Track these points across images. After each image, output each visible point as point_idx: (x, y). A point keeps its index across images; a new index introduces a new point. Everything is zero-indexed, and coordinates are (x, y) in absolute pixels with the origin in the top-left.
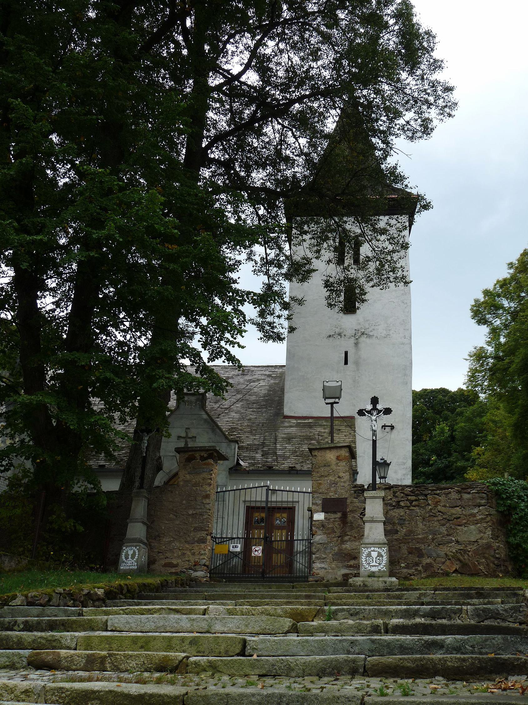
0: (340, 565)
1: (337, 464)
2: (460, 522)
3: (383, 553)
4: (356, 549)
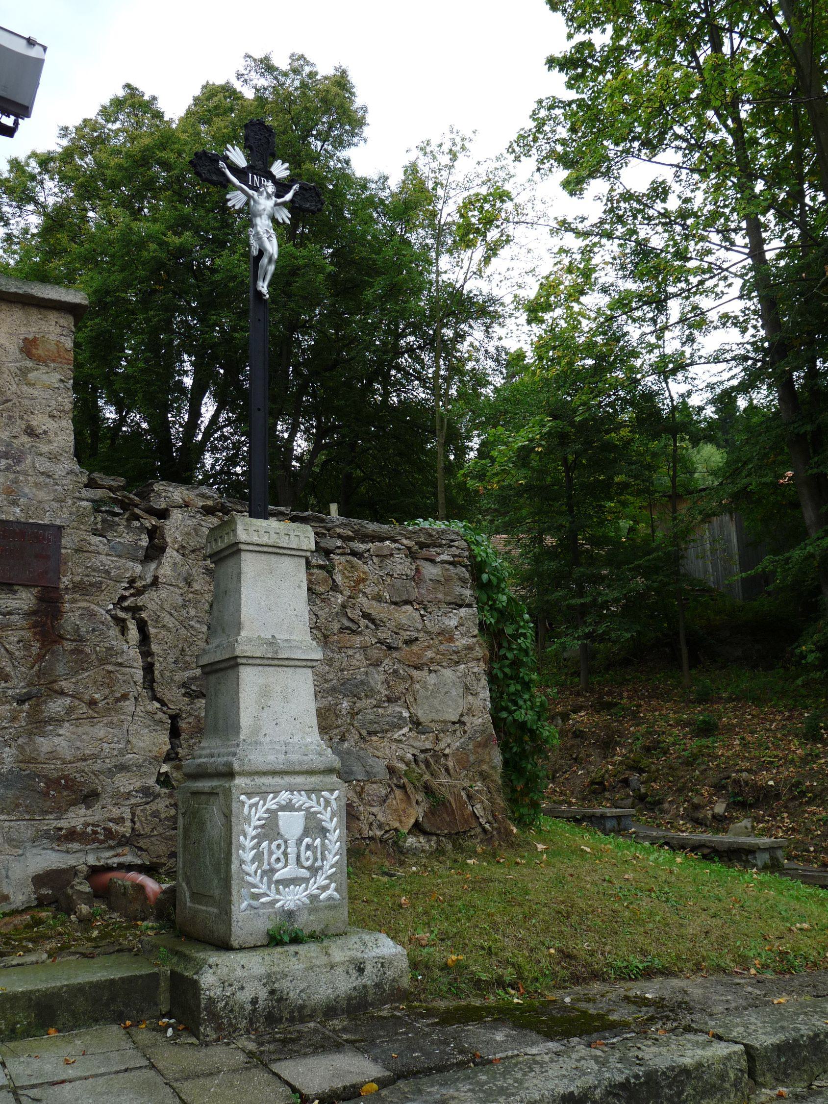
0: (24, 829)
1: (24, 372)
2: (419, 657)
3: (326, 816)
4: (95, 757)
